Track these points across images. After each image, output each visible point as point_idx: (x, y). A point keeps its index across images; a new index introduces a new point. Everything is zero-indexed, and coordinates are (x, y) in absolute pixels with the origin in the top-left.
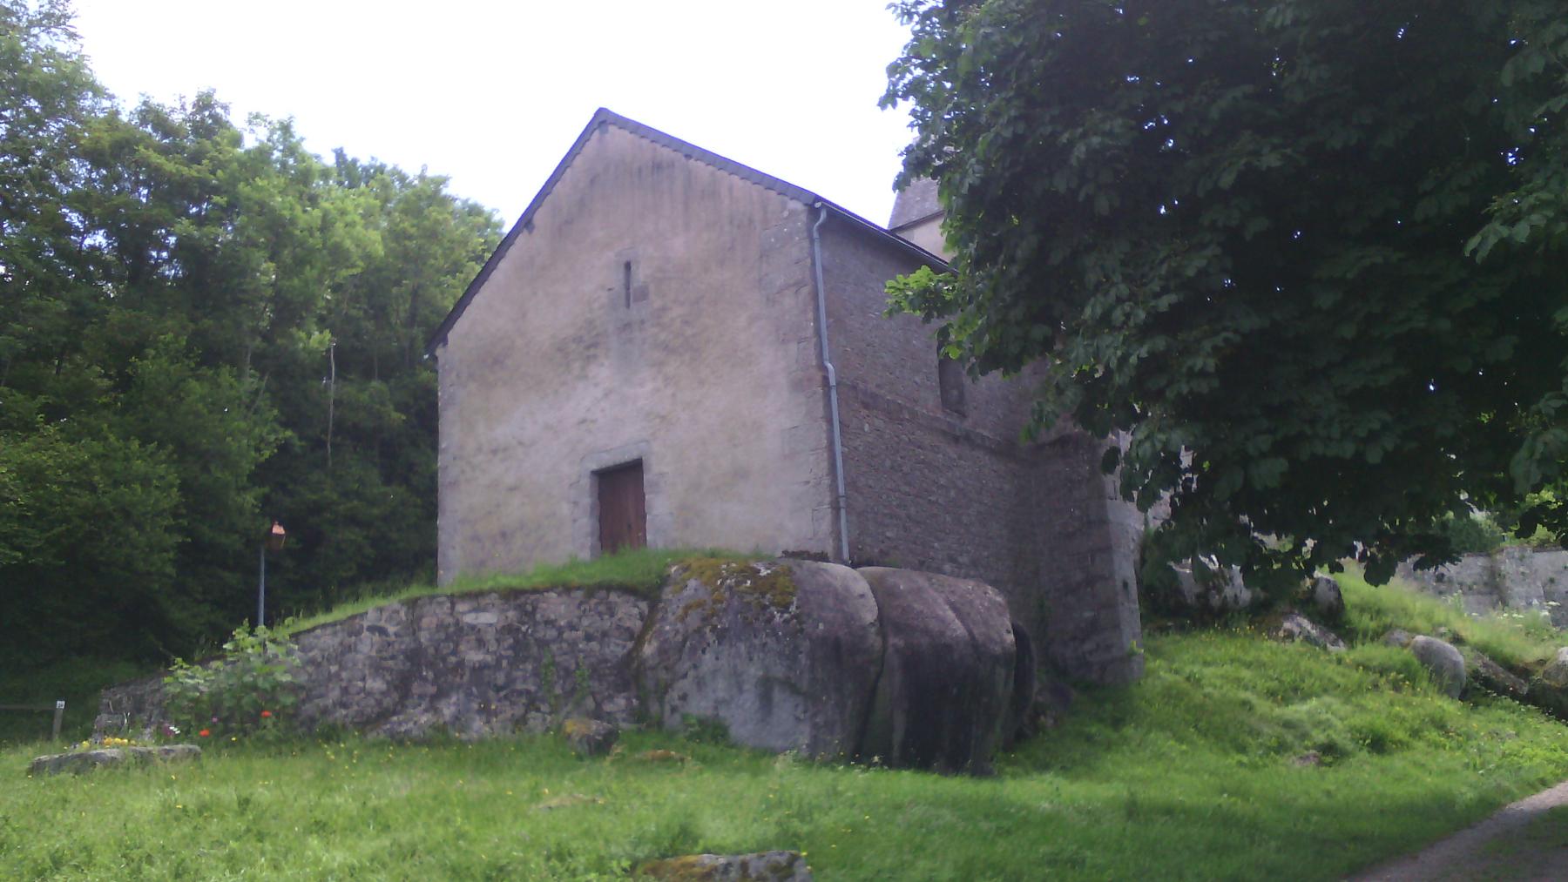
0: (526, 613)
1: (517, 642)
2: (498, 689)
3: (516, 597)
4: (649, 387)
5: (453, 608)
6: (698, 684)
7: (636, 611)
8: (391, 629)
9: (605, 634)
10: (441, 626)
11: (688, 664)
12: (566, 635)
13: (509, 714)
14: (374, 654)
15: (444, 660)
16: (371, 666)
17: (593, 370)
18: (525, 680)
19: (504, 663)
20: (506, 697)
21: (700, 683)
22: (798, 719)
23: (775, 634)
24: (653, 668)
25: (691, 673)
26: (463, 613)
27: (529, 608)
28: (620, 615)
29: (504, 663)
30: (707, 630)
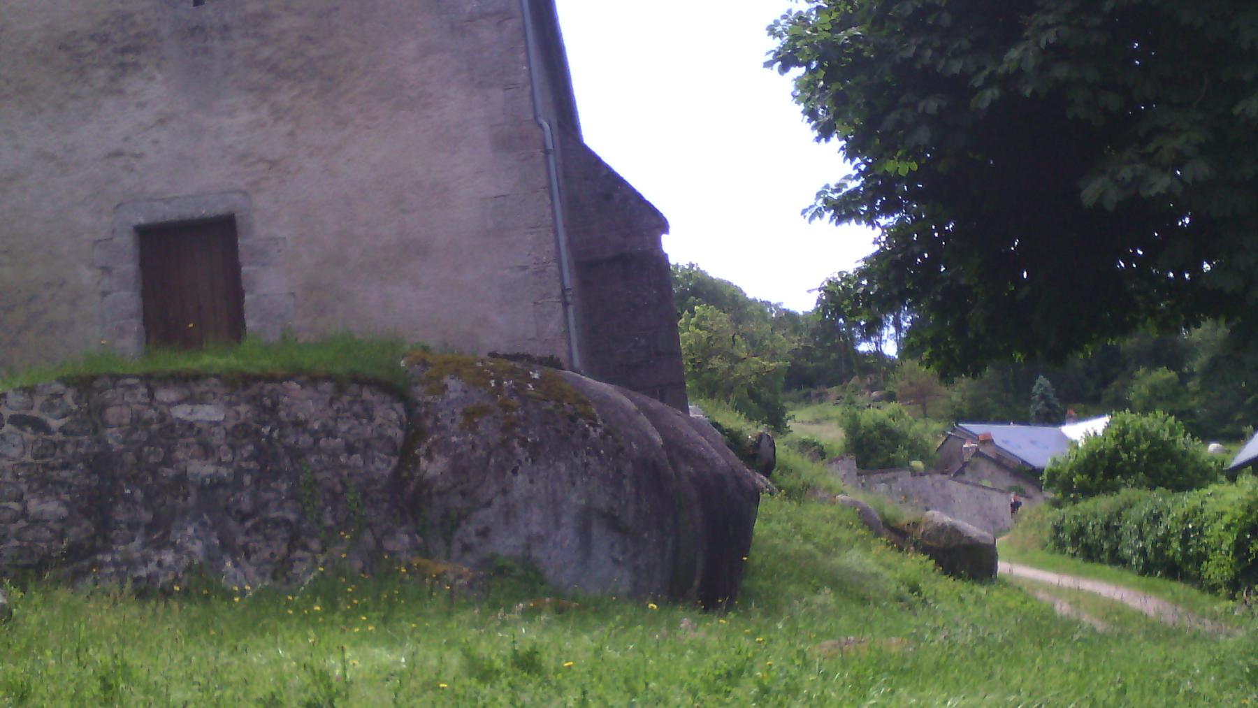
0: (264, 408)
1: (259, 448)
2: (244, 517)
3: (246, 386)
4: (245, 117)
5: (151, 394)
6: (507, 515)
7: (394, 416)
8: (55, 423)
9: (367, 445)
10: (138, 422)
11: (494, 488)
12: (323, 442)
13: (266, 554)
14: (28, 458)
15: (153, 470)
16: (29, 478)
17: (133, 83)
18: (281, 506)
19: (247, 479)
20: (256, 528)
21: (509, 513)
22: (616, 562)
23: (598, 453)
24: (440, 493)
25: (498, 501)
26: (171, 404)
27: (268, 402)
28: (379, 420)
29: (247, 479)
30: (515, 443)
